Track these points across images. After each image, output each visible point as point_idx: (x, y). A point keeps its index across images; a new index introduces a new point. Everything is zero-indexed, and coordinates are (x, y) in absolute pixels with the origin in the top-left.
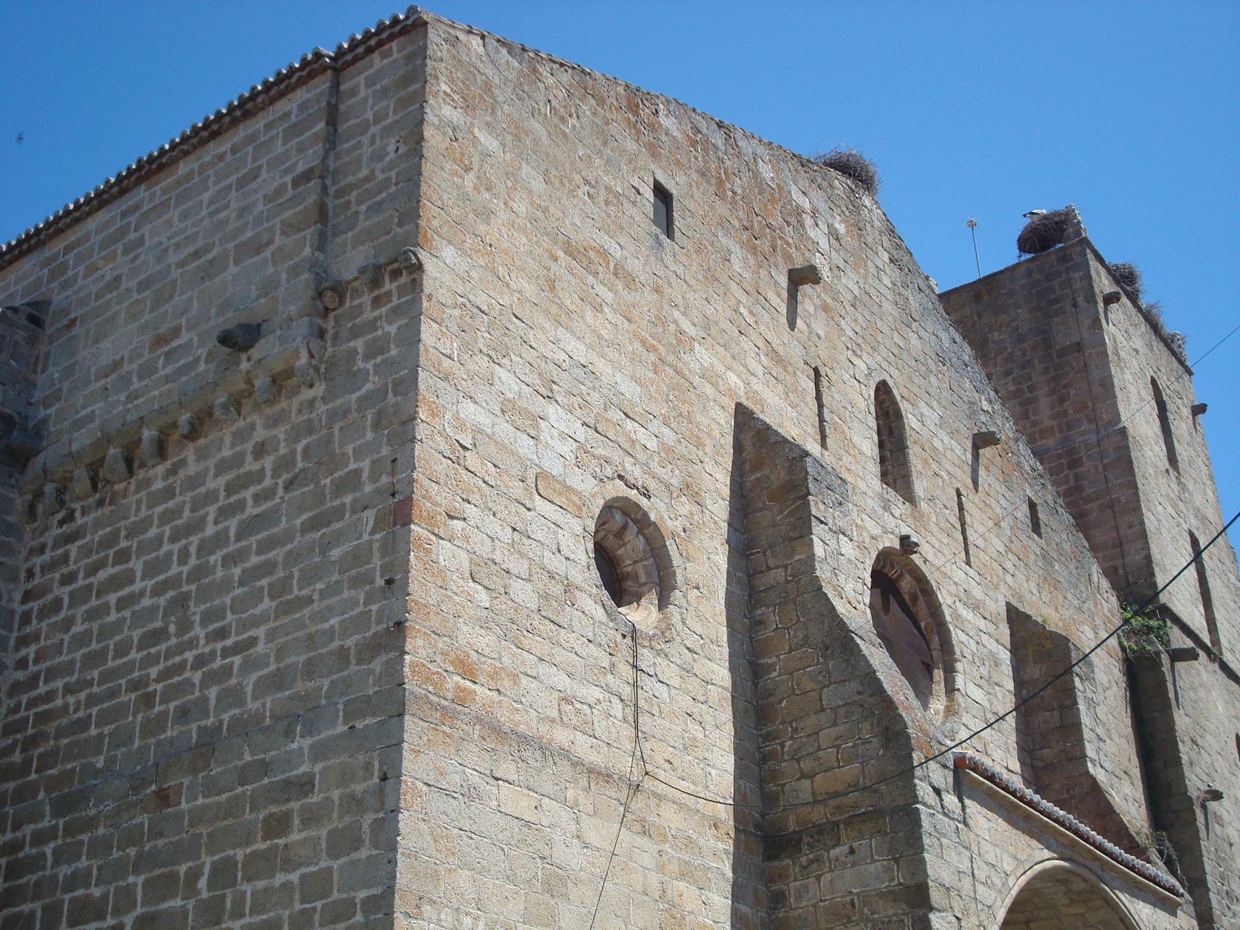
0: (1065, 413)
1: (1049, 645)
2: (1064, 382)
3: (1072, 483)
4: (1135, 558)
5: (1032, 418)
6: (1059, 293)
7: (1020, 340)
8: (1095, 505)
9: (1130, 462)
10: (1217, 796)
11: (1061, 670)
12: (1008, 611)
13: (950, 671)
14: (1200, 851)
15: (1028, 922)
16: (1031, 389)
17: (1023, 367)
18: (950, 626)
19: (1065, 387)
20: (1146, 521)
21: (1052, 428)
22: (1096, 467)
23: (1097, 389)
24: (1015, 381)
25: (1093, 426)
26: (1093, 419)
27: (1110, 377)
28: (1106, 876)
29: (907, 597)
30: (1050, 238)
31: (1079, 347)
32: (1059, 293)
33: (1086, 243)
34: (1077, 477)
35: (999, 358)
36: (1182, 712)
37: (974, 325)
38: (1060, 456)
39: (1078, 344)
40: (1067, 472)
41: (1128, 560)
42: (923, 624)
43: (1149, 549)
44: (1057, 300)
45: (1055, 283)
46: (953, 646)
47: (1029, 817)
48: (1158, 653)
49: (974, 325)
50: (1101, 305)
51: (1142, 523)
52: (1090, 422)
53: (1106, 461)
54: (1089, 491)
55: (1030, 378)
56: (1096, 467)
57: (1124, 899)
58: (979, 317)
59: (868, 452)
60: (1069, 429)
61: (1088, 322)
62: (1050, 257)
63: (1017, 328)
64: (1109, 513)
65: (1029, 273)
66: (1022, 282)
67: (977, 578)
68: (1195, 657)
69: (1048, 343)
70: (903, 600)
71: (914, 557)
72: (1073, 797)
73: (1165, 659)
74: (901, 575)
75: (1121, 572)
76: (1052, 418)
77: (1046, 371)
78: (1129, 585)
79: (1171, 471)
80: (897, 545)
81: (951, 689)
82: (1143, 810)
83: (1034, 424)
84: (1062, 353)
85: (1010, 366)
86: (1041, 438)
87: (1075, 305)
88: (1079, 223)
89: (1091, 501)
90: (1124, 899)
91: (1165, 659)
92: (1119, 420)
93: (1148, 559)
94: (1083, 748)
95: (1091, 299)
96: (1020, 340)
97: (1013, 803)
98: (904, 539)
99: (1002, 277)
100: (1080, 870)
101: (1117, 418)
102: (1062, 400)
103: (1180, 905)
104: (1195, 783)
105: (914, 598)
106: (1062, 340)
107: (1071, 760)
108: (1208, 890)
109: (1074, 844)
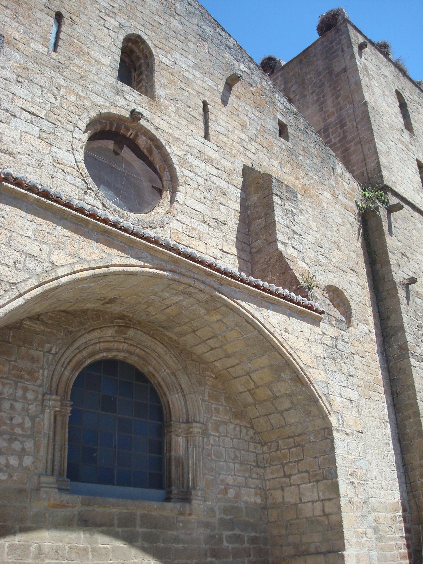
0: (339, 103)
1: (262, 182)
2: (338, 89)
3: (342, 136)
4: (371, 165)
5: (324, 110)
6: (335, 48)
7: (319, 75)
8: (352, 144)
9: (369, 117)
10: (413, 281)
11: (267, 194)
12: (244, 169)
13: (174, 192)
14: (401, 310)
15: (194, 331)
16: (323, 97)
17: (320, 87)
18: (177, 167)
19: (339, 91)
20: (377, 145)
21: (333, 112)
22: (353, 125)
23: (353, 87)
24: (317, 95)
25: (352, 106)
26: (352, 103)
27: (359, 79)
28: (223, 288)
29: (145, 151)
30: (331, 24)
31: (345, 70)
32: (335, 48)
33: (346, 21)
34: (344, 132)
35: (310, 86)
36: (394, 238)
37: (299, 75)
38: (336, 124)
39: (345, 69)
40: (339, 130)
41: (369, 167)
42: (158, 167)
43: (378, 158)
44: (335, 52)
45: (334, 44)
46: (177, 177)
47: (105, 232)
48: (377, 208)
49: (299, 75)
50: (356, 49)
51: (375, 146)
52: (350, 104)
53: (357, 120)
54: (349, 138)
55: (323, 91)
56: (353, 125)
57: (249, 308)
58: (301, 70)
59: (106, 60)
60: (341, 110)
61: (349, 57)
62: (331, 34)
63: (318, 70)
64: (359, 146)
65: (323, 43)
66: (320, 48)
67: (215, 148)
68: (401, 208)
69: (331, 73)
70: (142, 152)
71: (142, 122)
72: (269, 266)
73: (383, 211)
74: (136, 136)
75: (365, 174)
76: (333, 107)
77: (330, 86)
78: (369, 180)
79: (405, 130)
80: (127, 115)
81: (173, 200)
82: (367, 291)
83: (325, 112)
84: (339, 74)
85: (314, 88)
86: (328, 118)
87: (343, 51)
88: (344, 13)
89: (351, 142)
90: (249, 308)
91: (383, 211)
92: (364, 99)
93: (378, 164)
94: (275, 235)
95: (350, 46)
96: (319, 75)
97: (74, 216)
98: (133, 112)
99: (311, 49)
100: (177, 277)
101: (363, 98)
102: (337, 97)
103: (322, 319)
104: (399, 274)
105: (150, 151)
106: (337, 69)
107: (269, 244)
108: (405, 332)
109: (176, 262)
